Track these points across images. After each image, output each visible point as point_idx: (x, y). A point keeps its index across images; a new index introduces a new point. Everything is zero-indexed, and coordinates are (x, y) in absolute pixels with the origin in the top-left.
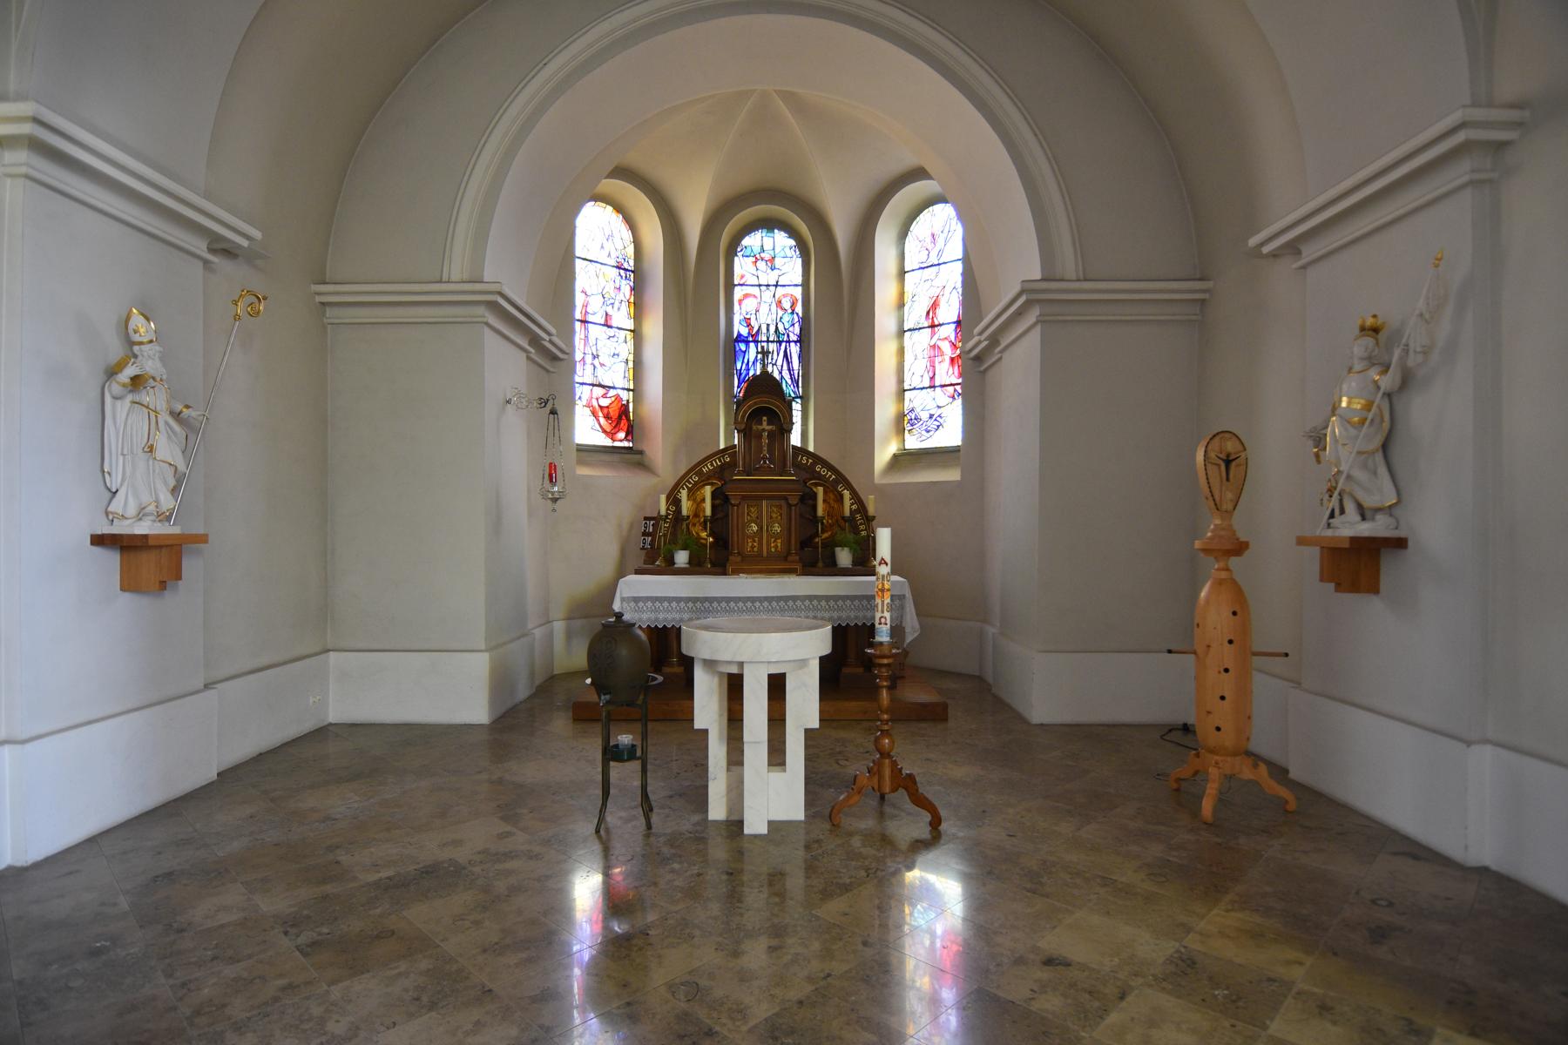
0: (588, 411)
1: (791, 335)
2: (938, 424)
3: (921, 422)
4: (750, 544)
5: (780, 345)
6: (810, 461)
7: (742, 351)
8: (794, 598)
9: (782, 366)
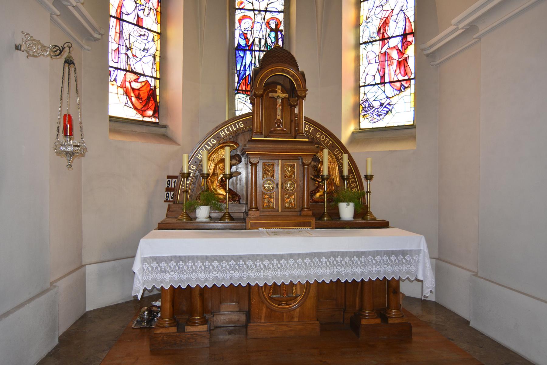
0: (121, 91)
2: (387, 110)
3: (374, 109)
4: (266, 200)
6: (312, 128)
7: (241, 57)
8: (319, 255)
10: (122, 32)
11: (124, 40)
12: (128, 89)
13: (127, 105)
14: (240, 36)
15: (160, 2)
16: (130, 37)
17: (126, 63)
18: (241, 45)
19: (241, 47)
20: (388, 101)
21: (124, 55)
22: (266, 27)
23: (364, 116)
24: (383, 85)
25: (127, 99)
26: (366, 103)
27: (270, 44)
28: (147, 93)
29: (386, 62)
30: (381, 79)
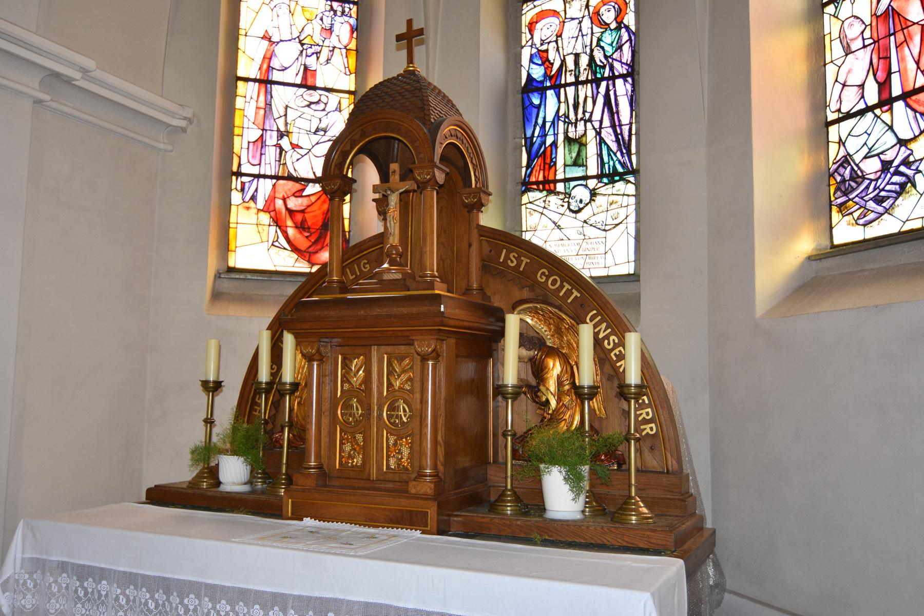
0: (265, 218)
1: (617, 65)
2: (902, 179)
5: (598, 87)
9: (601, 122)
10: (271, 105)
11: (275, 120)
12: (280, 213)
13: (276, 244)
14: (531, 61)
15: (356, 29)
16: (286, 112)
17: (277, 162)
18: (535, 79)
19: (535, 84)
20: (904, 152)
21: (274, 147)
22: (592, 23)
23: (842, 208)
24: (885, 108)
25: (276, 232)
26: (844, 170)
27: (601, 61)
28: (322, 217)
29: (892, 38)
30: (880, 93)
